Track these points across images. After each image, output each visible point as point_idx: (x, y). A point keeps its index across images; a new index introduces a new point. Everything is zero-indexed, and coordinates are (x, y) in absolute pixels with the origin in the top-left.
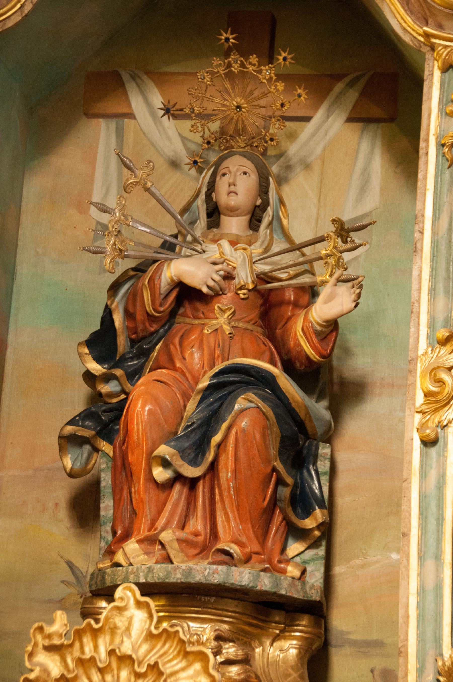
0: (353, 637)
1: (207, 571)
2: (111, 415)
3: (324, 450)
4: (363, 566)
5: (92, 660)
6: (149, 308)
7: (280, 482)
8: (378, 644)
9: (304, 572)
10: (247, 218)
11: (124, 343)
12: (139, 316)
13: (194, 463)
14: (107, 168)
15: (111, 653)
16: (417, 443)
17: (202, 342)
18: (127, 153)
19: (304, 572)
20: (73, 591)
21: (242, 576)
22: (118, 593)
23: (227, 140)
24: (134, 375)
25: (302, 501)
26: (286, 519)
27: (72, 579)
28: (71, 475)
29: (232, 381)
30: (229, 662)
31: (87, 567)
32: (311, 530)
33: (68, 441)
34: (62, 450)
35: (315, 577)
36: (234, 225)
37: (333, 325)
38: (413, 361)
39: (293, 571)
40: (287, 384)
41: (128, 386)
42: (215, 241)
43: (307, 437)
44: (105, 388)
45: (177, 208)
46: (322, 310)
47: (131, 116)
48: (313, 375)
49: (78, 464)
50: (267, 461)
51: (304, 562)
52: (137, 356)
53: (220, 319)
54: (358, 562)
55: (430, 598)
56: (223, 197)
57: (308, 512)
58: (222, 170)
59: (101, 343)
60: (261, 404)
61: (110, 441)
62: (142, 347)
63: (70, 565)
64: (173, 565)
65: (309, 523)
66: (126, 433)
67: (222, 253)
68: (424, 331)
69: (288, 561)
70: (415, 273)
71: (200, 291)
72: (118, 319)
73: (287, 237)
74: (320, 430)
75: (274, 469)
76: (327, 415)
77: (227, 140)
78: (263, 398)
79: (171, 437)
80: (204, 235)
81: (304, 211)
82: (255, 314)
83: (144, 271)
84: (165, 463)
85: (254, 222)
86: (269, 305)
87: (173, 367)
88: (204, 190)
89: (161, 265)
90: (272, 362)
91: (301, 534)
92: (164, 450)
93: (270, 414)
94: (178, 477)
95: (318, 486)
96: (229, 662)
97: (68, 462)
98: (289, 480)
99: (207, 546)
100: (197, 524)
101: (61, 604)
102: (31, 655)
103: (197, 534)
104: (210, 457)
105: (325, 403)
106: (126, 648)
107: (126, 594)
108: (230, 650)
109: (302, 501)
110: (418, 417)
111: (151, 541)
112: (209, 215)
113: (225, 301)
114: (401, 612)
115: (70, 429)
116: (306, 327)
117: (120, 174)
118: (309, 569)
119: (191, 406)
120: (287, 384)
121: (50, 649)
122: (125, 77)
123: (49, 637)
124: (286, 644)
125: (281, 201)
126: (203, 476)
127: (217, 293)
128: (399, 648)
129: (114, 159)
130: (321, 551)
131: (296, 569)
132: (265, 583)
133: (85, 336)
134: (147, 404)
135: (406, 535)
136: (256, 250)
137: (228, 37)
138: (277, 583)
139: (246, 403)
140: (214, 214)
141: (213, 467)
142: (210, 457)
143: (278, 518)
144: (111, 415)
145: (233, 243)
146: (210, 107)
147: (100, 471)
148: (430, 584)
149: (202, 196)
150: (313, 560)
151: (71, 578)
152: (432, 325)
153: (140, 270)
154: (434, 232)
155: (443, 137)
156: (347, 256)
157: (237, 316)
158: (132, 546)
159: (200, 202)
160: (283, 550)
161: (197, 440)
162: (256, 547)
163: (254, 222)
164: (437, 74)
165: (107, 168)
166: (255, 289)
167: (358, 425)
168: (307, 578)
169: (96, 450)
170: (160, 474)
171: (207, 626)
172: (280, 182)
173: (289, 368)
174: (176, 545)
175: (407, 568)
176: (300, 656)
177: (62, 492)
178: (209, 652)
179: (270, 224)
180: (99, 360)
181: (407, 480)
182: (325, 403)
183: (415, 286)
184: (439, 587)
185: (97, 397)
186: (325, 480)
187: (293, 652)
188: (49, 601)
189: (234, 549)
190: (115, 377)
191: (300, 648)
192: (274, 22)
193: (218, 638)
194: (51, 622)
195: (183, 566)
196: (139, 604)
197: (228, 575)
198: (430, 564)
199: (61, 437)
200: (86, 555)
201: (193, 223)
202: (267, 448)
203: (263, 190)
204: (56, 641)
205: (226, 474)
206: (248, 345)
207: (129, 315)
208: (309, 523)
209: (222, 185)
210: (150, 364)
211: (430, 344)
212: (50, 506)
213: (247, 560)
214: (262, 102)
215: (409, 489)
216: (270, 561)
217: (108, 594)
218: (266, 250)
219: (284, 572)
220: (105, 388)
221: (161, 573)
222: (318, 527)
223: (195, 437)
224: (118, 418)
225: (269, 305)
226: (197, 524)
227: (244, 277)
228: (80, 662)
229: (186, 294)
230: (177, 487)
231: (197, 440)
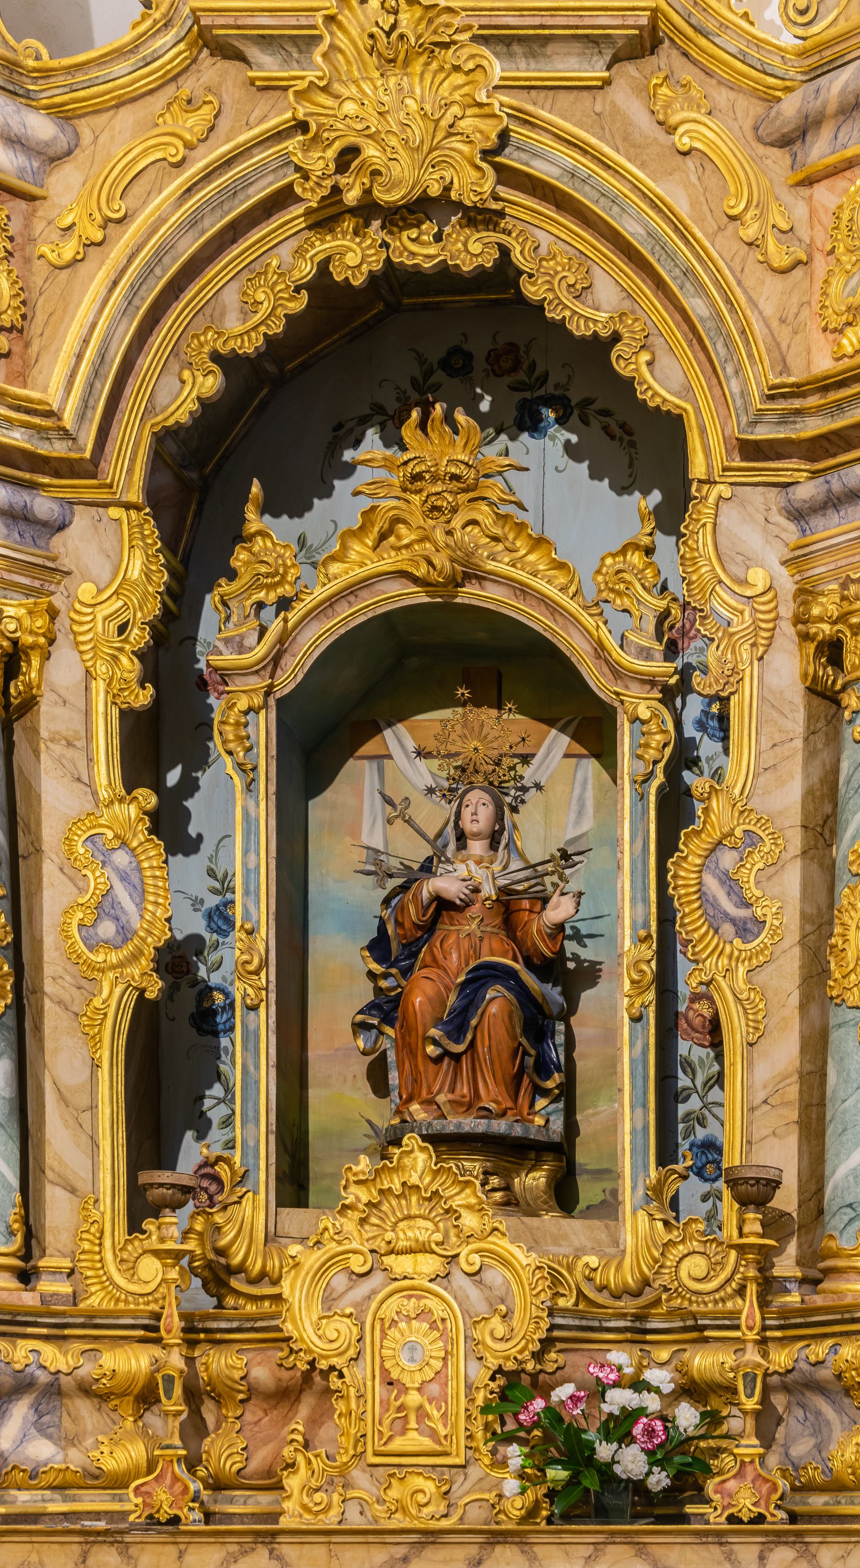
0: (589, 1167)
1: (471, 1124)
2: (391, 1005)
3: (560, 1027)
4: (594, 1115)
5: (390, 1189)
6: (414, 918)
7: (525, 1053)
8: (607, 1171)
9: (547, 1121)
10: (487, 841)
11: (395, 949)
12: (407, 925)
13: (457, 1041)
14: (373, 801)
15: (404, 1184)
16: (626, 1020)
17: (458, 945)
18: (388, 793)
19: (547, 1121)
20: (374, 1142)
21: (500, 1126)
22: (405, 1141)
24: (406, 972)
25: (543, 1068)
26: (531, 1081)
27: (371, 1132)
28: (364, 1053)
29: (483, 976)
30: (494, 1190)
31: (382, 1124)
32: (551, 1090)
33: (359, 1027)
34: (355, 1033)
35: (557, 1125)
36: (477, 847)
38: (621, 956)
39: (539, 1121)
40: (529, 979)
41: (404, 983)
42: (463, 861)
43: (545, 1016)
44: (384, 984)
45: (431, 835)
47: (389, 757)
49: (369, 1045)
50: (514, 1038)
51: (549, 1114)
52: (407, 958)
53: (470, 925)
54: (591, 1111)
55: (640, 1136)
56: (468, 825)
57: (548, 1076)
58: (465, 803)
59: (379, 947)
60: (507, 993)
61: (393, 1027)
62: (411, 950)
63: (369, 1122)
65: (550, 1084)
66: (404, 1018)
67: (469, 871)
68: (628, 932)
69: (536, 1113)
70: (619, 885)
71: (454, 903)
72: (390, 929)
73: (522, 856)
74: (555, 1011)
75: (520, 1044)
76: (560, 999)
78: (509, 989)
79: (438, 1022)
80: (455, 856)
81: (537, 833)
82: (498, 921)
83: (408, 888)
84: (435, 1043)
87: (439, 967)
88: (453, 818)
89: (421, 883)
90: (515, 959)
91: (545, 1093)
92: (434, 1032)
93: (514, 1001)
94: (446, 1053)
95: (557, 1055)
96: (494, 1190)
97: (361, 1044)
98: (533, 1052)
99: (470, 1106)
101: (365, 1151)
102: (345, 1188)
103: (463, 1096)
104: (469, 1037)
105: (559, 989)
106: (414, 1179)
107: (411, 1140)
108: (495, 1181)
109: (543, 1068)
110: (626, 1000)
111: (430, 1102)
112: (458, 839)
113: (475, 910)
114: (619, 1147)
115: (360, 1018)
117: (384, 811)
118: (552, 1118)
119: (452, 998)
121: (358, 1182)
122: (382, 724)
123: (355, 1174)
124: (536, 1174)
125: (515, 826)
126: (465, 1052)
127: (467, 904)
129: (378, 797)
130: (561, 1105)
131: (544, 1118)
132: (518, 1131)
133: (366, 943)
135: (621, 1090)
136: (497, 867)
137: (462, 692)
138: (527, 1130)
140: (462, 838)
141: (472, 1045)
142: (469, 1037)
143: (526, 1081)
144: (391, 1005)
145: (478, 863)
146: (453, 749)
147: (385, 1051)
148: (639, 1126)
149: (451, 824)
150: (554, 1112)
151: (371, 1132)
152: (634, 927)
153: (404, 888)
154: (632, 854)
156: (568, 872)
157: (486, 922)
158: (415, 1107)
159: (450, 828)
160: (532, 1105)
161: (458, 1023)
162: (510, 1104)
164: (627, 725)
165: (373, 801)
166: (497, 900)
168: (551, 1125)
169: (382, 1033)
170: (430, 1049)
171: (477, 1164)
172: (514, 810)
173: (528, 963)
174: (448, 1106)
175: (623, 1114)
176: (548, 1184)
177: (360, 1066)
178: (478, 1183)
179: (507, 845)
180: (378, 961)
181: (620, 1049)
182: (559, 989)
183: (619, 896)
184: (646, 1128)
185: (378, 991)
186: (561, 1050)
187: (543, 1180)
188: (356, 1150)
189: (492, 1106)
190: (391, 975)
191: (547, 1178)
192: (500, 675)
193: (485, 1173)
194: (357, 1163)
195: (455, 1121)
196: (422, 1149)
197: (489, 1126)
198: (639, 1111)
199: (353, 1024)
200: (382, 1114)
201: (445, 846)
202: (513, 1028)
203: (499, 817)
204: (362, 1177)
205: (482, 1048)
206: (496, 945)
207: (399, 924)
208: (550, 1084)
209: (466, 814)
210: (418, 964)
211: (633, 942)
212: (350, 1078)
213: (503, 1114)
214: (495, 745)
215: (622, 1055)
216: (521, 1114)
217: (397, 1143)
218: (505, 868)
219: (532, 1121)
220: (384, 984)
221: (438, 1126)
222: (557, 1087)
223: (456, 1022)
224: (396, 1008)
225: (508, 908)
227: (488, 890)
228: (381, 1192)
229: (443, 906)
230: (446, 1060)
231: (458, 1023)
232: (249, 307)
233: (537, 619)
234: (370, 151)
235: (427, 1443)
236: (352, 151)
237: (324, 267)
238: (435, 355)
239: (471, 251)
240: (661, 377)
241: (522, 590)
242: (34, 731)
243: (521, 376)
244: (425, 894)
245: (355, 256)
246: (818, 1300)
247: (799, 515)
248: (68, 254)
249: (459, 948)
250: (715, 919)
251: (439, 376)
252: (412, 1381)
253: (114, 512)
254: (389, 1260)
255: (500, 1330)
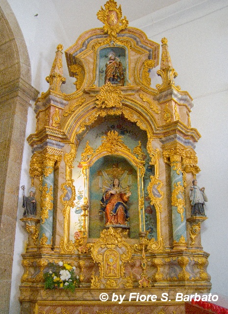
1: (118, 225)
21: (122, 226)
23: (114, 177)
24: (106, 204)
25: (127, 217)
36: (116, 186)
37: (129, 197)
40: (124, 204)
46: (127, 196)
48: (126, 202)
56: (115, 184)
64: (173, 78)
77: (114, 177)
81: (124, 184)
84: (112, 214)
85: (118, 186)
86: (121, 196)
100: (116, 220)
109: (127, 217)
116: (181, 99)
120: (124, 204)
128: (47, 136)
134: (109, 207)
139: (120, 207)
140: (114, 185)
141: (117, 214)
155: (185, 100)
158: (108, 223)
163: (118, 186)
167: (132, 207)
207: (105, 197)
209: (115, 182)
225: (121, 196)
226: (116, 220)
229: (112, 195)
232: (89, 119)
233: (125, 156)
234: (106, 102)
235: (114, 275)
236: (104, 102)
237: (99, 115)
238: (110, 126)
239: (119, 113)
240: (142, 126)
241: (123, 153)
242: (58, 172)
243: (121, 128)
244: (109, 193)
245: (104, 114)
246: (172, 251)
247: (162, 142)
248: (66, 115)
249: (115, 201)
250: (154, 195)
251: (111, 128)
252: (112, 264)
253: (70, 144)
254: (108, 246)
255: (125, 256)
